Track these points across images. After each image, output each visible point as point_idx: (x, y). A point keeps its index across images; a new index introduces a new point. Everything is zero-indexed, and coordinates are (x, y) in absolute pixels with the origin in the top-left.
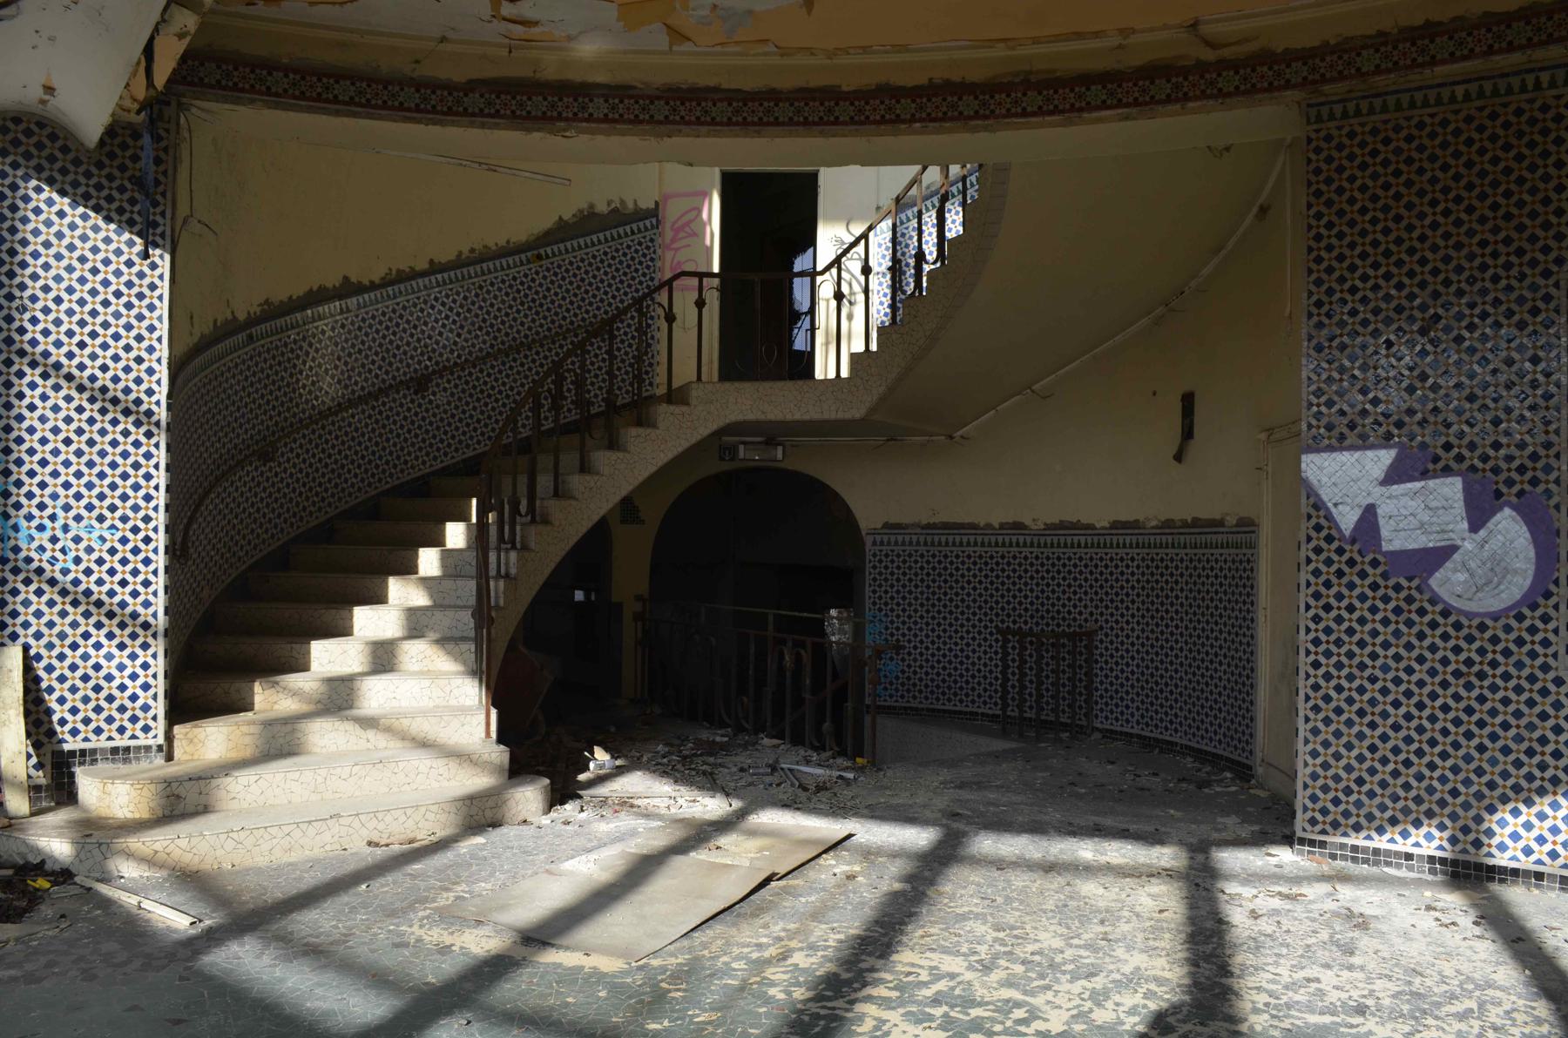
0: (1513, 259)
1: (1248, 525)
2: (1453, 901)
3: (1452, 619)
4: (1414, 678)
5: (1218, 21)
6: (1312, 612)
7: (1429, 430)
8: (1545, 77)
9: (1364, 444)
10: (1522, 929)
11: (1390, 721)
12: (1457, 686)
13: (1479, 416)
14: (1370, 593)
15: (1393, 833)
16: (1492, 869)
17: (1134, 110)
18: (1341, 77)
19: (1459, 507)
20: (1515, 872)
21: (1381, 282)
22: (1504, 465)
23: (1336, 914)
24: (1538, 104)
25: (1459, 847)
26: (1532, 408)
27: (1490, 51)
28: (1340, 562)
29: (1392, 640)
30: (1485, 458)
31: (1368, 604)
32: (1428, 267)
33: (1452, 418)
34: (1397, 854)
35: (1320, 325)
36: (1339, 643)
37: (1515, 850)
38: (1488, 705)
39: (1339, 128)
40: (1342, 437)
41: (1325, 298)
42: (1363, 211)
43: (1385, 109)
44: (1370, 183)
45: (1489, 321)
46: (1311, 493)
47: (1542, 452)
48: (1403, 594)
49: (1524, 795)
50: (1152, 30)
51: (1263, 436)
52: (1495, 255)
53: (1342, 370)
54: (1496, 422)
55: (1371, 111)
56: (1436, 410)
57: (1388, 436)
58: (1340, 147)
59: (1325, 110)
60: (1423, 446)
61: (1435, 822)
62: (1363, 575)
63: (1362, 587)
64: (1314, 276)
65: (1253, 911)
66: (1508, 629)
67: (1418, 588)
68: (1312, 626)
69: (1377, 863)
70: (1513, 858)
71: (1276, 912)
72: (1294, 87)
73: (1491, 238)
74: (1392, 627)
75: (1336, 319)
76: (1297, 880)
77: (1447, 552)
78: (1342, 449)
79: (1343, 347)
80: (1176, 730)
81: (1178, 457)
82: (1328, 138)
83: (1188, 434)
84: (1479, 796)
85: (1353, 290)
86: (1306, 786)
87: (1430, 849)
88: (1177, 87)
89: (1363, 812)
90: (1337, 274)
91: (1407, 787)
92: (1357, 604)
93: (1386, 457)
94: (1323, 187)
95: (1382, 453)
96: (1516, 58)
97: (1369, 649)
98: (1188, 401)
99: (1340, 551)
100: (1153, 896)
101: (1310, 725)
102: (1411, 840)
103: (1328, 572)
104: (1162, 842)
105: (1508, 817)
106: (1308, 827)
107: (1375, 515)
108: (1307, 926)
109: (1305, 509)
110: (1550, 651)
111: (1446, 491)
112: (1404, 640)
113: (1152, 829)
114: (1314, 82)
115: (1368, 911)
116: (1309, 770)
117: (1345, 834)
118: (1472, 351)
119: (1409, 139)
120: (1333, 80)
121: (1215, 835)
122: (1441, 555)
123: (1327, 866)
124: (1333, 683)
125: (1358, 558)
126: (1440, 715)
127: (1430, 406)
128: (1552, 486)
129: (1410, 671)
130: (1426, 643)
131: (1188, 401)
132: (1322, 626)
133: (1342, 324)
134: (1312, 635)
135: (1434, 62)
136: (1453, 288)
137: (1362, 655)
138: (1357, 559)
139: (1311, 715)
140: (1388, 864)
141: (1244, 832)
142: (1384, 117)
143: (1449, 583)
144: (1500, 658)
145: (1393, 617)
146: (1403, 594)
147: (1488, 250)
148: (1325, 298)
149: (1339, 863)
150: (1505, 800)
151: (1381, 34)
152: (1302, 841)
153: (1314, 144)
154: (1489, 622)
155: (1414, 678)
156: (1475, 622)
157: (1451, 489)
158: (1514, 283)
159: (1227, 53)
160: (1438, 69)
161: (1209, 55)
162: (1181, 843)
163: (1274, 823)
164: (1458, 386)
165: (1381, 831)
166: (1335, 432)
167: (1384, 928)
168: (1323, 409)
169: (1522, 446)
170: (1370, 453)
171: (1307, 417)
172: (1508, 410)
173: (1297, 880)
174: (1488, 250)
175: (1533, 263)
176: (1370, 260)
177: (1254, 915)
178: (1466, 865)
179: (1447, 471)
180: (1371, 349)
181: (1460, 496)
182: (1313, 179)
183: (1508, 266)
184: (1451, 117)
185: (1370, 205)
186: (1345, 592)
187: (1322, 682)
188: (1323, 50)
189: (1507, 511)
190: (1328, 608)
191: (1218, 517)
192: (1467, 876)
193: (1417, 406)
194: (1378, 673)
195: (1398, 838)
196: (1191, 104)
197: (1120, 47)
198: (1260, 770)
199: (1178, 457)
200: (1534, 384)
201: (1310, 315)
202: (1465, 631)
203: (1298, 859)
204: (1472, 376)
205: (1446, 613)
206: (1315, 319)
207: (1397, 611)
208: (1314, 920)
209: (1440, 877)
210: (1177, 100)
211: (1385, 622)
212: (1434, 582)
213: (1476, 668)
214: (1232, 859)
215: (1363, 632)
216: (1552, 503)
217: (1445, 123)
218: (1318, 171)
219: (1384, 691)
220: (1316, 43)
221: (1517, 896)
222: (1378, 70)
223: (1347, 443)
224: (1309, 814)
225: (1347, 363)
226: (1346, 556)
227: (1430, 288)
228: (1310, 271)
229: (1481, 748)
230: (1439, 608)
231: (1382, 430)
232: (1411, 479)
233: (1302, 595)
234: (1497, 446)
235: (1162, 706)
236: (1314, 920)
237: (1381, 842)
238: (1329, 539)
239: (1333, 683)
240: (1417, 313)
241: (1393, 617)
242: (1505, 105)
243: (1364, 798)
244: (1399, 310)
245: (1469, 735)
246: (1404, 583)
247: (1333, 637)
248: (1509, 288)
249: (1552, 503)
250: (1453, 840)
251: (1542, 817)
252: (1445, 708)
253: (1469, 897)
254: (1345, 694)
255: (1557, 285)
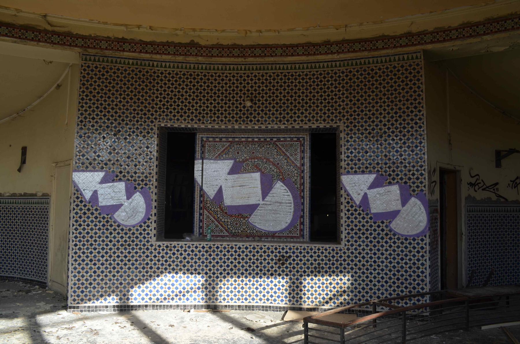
0: (143, 116)
1: (46, 196)
2: (122, 319)
3: (121, 228)
4: (109, 247)
5: (54, 17)
6: (74, 227)
7: (115, 166)
8: (155, 63)
9: (94, 170)
10: (145, 324)
11: (101, 262)
12: (122, 249)
13: (131, 163)
14: (94, 220)
15: (102, 300)
16: (132, 306)
17: (19, 40)
18: (94, 48)
19: (124, 192)
20: (139, 306)
21: (103, 117)
22: (137, 179)
23: (87, 332)
24: (153, 71)
25: (292, 303)
26: (146, 162)
27: (141, 52)
28: (85, 210)
29: (102, 235)
30: (132, 177)
31: (94, 223)
32: (118, 115)
33: (122, 163)
34: (103, 307)
35: (81, 129)
36: (84, 237)
37: (139, 299)
38: (131, 254)
39: (93, 64)
40: (87, 167)
41: (84, 120)
42: (98, 93)
43: (107, 62)
44: (101, 84)
45: (135, 134)
46: (75, 185)
47: (148, 175)
48: (105, 220)
49: (142, 281)
50: (29, 13)
51: (54, 165)
52: (138, 114)
53: (88, 144)
54: (136, 166)
55: (103, 61)
56: (117, 160)
57: (102, 168)
58: (92, 71)
59: (88, 57)
60: (113, 172)
61: (115, 294)
62: (92, 214)
63: (92, 218)
64: (80, 112)
65: (58, 337)
66: (137, 230)
67: (110, 218)
68: (75, 232)
69: (96, 311)
70: (309, 305)
71: (66, 335)
72: (79, 47)
73: (137, 108)
74: (102, 231)
75: (87, 127)
76: (71, 322)
77: (120, 206)
78: (87, 171)
79: (89, 137)
80: (15, 272)
81: (19, 170)
82: (88, 67)
83: (23, 162)
84: (129, 284)
85: (93, 118)
86: (72, 288)
87: (114, 303)
88: (36, 36)
89: (91, 294)
90: (88, 112)
91: (106, 284)
92: (90, 224)
93: (101, 174)
94: (86, 83)
95: (100, 173)
96: (148, 56)
97: (94, 239)
98: (24, 150)
99: (85, 206)
100: (18, 339)
101: (74, 266)
102: (107, 301)
103: (81, 213)
104: (17, 317)
105: (137, 289)
106: (73, 302)
107: (97, 194)
108: (78, 338)
109: (73, 191)
110: (149, 236)
111: (120, 186)
112: (105, 235)
113: (11, 312)
114: (85, 47)
115: (97, 328)
116: (73, 282)
117: (86, 303)
118: (129, 142)
119: (114, 73)
120: (91, 48)
121: (37, 310)
122: (117, 207)
123: (80, 315)
124: (82, 251)
125: (91, 208)
126: (117, 259)
127: (116, 159)
128: (151, 186)
129: (107, 245)
130: (113, 236)
131: (24, 150)
132: (78, 232)
133: (89, 129)
134: (75, 235)
135: (124, 50)
136: (125, 122)
137: (92, 241)
138: (89, 209)
139: (74, 263)
140: (100, 310)
141: (48, 307)
142: (137, 67)
143: (120, 216)
144: (135, 239)
145: (102, 228)
146: (105, 220)
147: (136, 112)
148: (84, 120)
149: (84, 313)
150: (136, 284)
151: (108, 37)
152: (70, 308)
153: (83, 68)
154: (132, 228)
155: (109, 247)
156: (128, 228)
157: (121, 186)
158: (143, 123)
159: (56, 29)
160: (125, 53)
161: (49, 28)
162: (24, 316)
163: (60, 302)
164: (125, 153)
165: (97, 299)
166: (85, 165)
167: (103, 333)
168: (81, 157)
169: (143, 173)
170: (96, 173)
171: (75, 159)
172: (139, 162)
173: (71, 322)
174: (136, 112)
175: (148, 118)
176: (99, 109)
177: (59, 338)
178: (125, 306)
179: (120, 180)
180: (98, 139)
181: (124, 188)
182: (82, 79)
183: (141, 118)
184: (128, 69)
185: (100, 92)
186: (86, 219)
187: (78, 251)
188: (89, 37)
189: (138, 193)
190: (80, 225)
191: (34, 193)
192: (125, 310)
193: (112, 159)
194: (97, 247)
195: (103, 301)
196: (41, 44)
197: (15, 15)
198: (50, 284)
199: (19, 170)
200: (147, 155)
201: (78, 125)
202: (124, 231)
203: (69, 314)
204: (129, 151)
205: (119, 226)
206: (80, 126)
207: (104, 225)
208: (80, 335)
209: (117, 312)
210: (36, 41)
211: (99, 229)
212: (115, 216)
213: (128, 243)
214: (43, 319)
215: (92, 233)
216: (151, 191)
217: (126, 70)
218: (84, 77)
219: (99, 253)
220: (87, 34)
221: (140, 314)
222: (106, 49)
223: (88, 169)
224: (73, 297)
225: (90, 142)
226: (87, 208)
227: (118, 121)
228: (79, 110)
229: (129, 268)
230: (117, 224)
231: (100, 166)
232: (109, 182)
233: (71, 221)
234: (135, 173)
235: (9, 264)
236: (80, 335)
237: (97, 303)
238: (81, 202)
239: (82, 251)
240: (113, 129)
241: (102, 228)
242: (144, 69)
243: (92, 289)
244: (108, 127)
245: (125, 264)
246: (106, 216)
247: (82, 235)
248: (141, 125)
249: (151, 191)
250: (121, 299)
251: (147, 287)
252: (118, 257)
253: (126, 317)
254: (86, 255)
255: (155, 126)
